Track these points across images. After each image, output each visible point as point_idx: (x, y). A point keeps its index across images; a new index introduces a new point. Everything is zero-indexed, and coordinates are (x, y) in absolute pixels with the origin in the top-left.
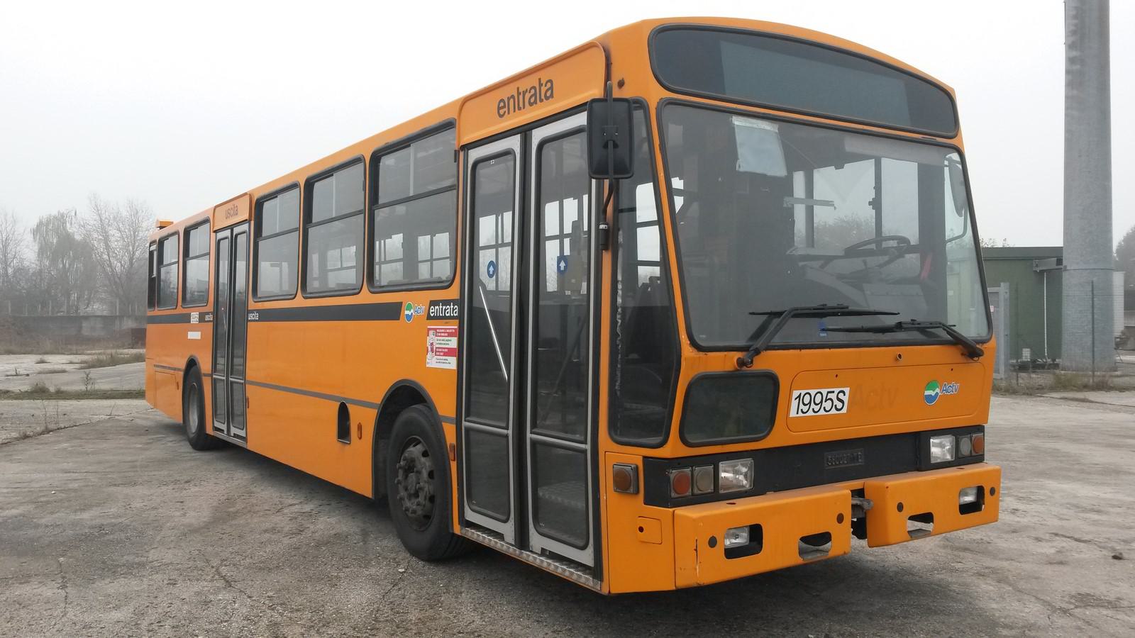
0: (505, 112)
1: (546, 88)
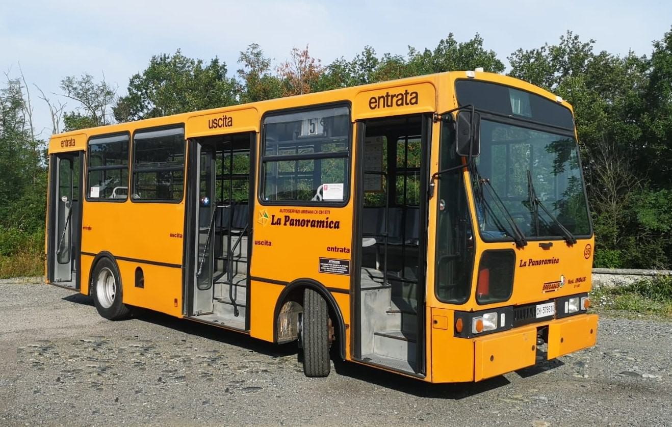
0: (376, 106)
1: (398, 99)
